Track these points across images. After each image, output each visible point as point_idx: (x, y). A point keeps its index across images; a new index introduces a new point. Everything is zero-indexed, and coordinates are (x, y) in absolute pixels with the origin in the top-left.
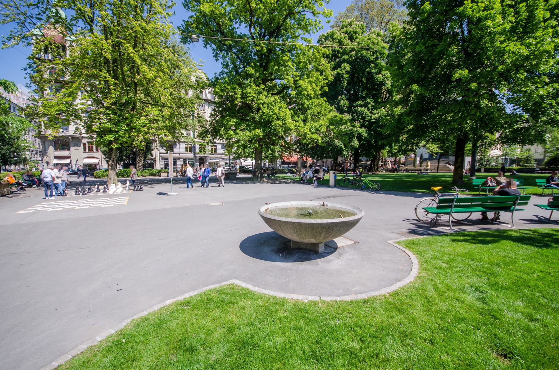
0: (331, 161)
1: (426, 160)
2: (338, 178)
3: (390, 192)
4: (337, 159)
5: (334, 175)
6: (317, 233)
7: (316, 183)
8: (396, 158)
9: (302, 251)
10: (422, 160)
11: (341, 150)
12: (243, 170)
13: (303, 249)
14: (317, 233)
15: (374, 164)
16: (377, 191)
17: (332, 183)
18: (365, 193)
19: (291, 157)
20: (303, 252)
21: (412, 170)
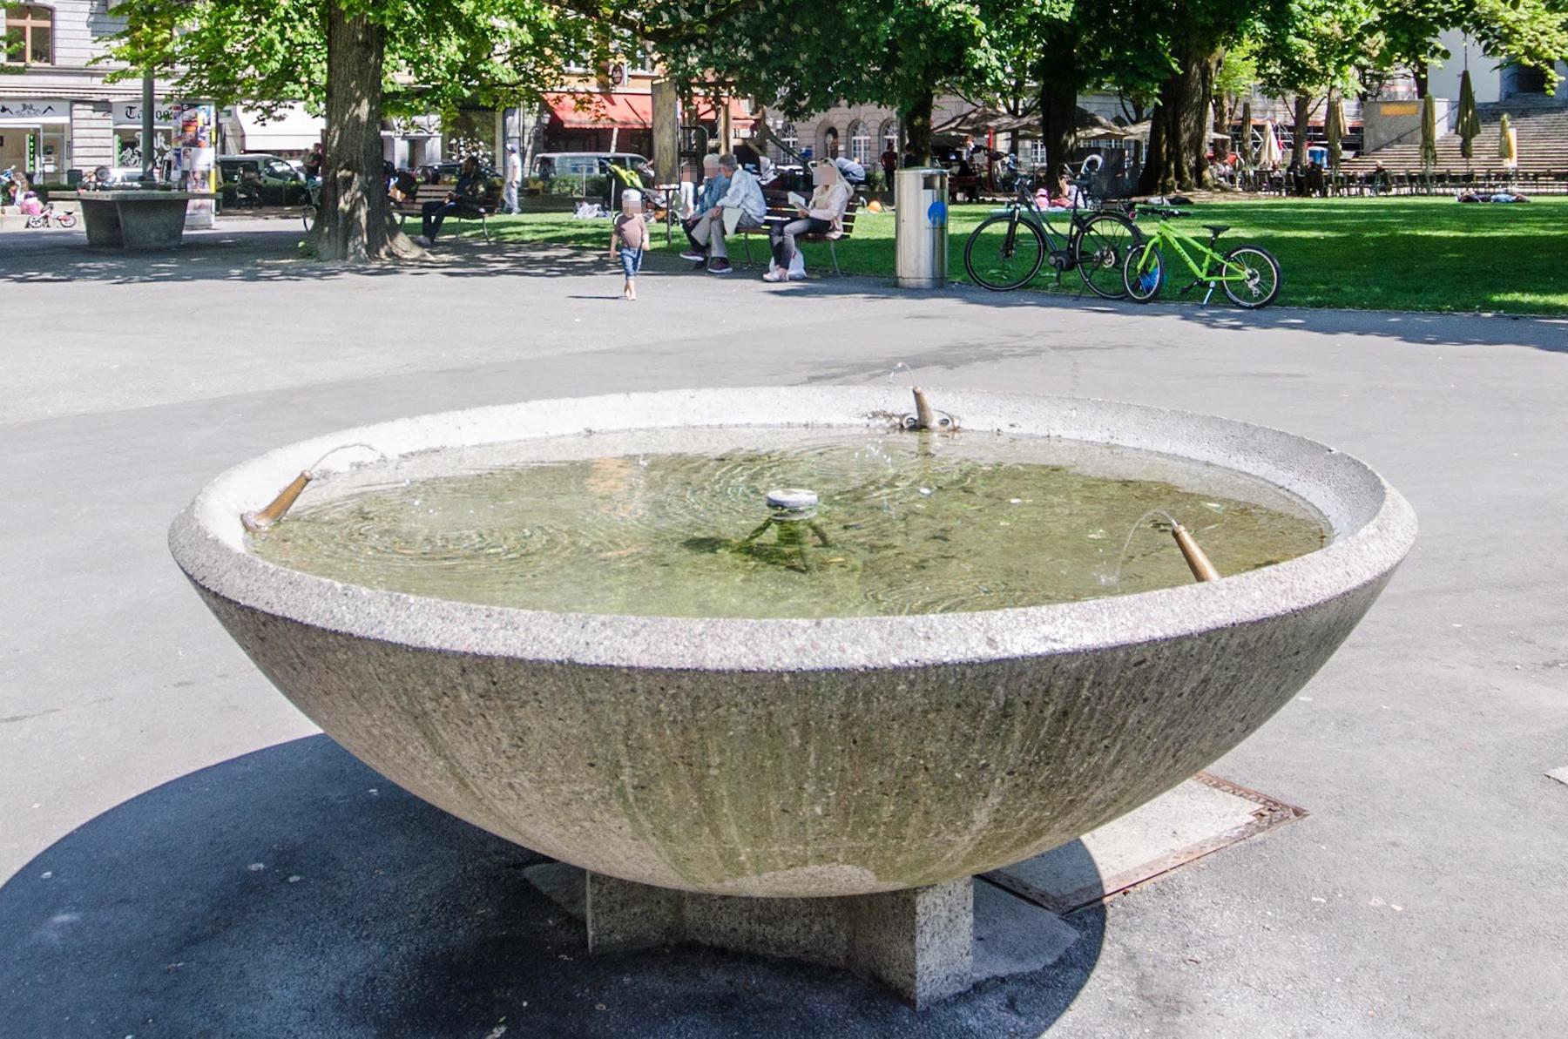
0: (885, 126)
1: (1492, 113)
2: (956, 227)
3: (1350, 315)
4: (923, 107)
5: (928, 198)
6: (906, 792)
7: (797, 266)
8: (1302, 104)
9: (718, 979)
10: (1471, 116)
11: (962, 38)
12: (248, 185)
13: (723, 955)
14: (906, 792)
15: (1174, 137)
16: (1267, 306)
17: (915, 259)
18: (1167, 326)
19: (606, 92)
20: (726, 1004)
21: (1412, 179)
